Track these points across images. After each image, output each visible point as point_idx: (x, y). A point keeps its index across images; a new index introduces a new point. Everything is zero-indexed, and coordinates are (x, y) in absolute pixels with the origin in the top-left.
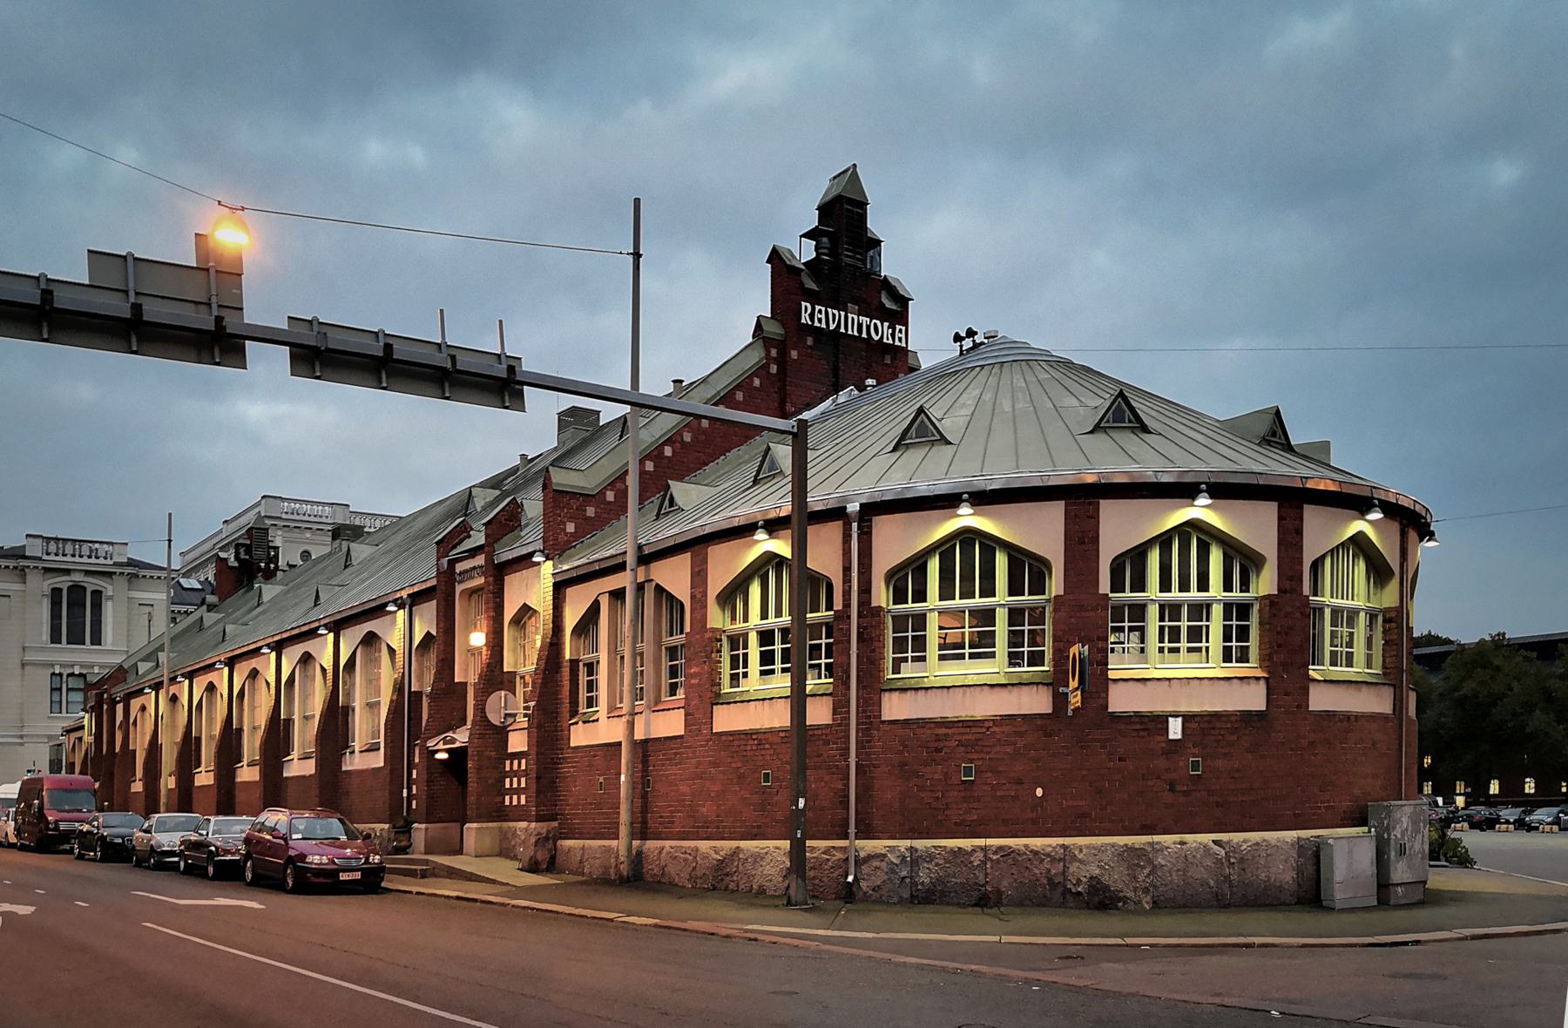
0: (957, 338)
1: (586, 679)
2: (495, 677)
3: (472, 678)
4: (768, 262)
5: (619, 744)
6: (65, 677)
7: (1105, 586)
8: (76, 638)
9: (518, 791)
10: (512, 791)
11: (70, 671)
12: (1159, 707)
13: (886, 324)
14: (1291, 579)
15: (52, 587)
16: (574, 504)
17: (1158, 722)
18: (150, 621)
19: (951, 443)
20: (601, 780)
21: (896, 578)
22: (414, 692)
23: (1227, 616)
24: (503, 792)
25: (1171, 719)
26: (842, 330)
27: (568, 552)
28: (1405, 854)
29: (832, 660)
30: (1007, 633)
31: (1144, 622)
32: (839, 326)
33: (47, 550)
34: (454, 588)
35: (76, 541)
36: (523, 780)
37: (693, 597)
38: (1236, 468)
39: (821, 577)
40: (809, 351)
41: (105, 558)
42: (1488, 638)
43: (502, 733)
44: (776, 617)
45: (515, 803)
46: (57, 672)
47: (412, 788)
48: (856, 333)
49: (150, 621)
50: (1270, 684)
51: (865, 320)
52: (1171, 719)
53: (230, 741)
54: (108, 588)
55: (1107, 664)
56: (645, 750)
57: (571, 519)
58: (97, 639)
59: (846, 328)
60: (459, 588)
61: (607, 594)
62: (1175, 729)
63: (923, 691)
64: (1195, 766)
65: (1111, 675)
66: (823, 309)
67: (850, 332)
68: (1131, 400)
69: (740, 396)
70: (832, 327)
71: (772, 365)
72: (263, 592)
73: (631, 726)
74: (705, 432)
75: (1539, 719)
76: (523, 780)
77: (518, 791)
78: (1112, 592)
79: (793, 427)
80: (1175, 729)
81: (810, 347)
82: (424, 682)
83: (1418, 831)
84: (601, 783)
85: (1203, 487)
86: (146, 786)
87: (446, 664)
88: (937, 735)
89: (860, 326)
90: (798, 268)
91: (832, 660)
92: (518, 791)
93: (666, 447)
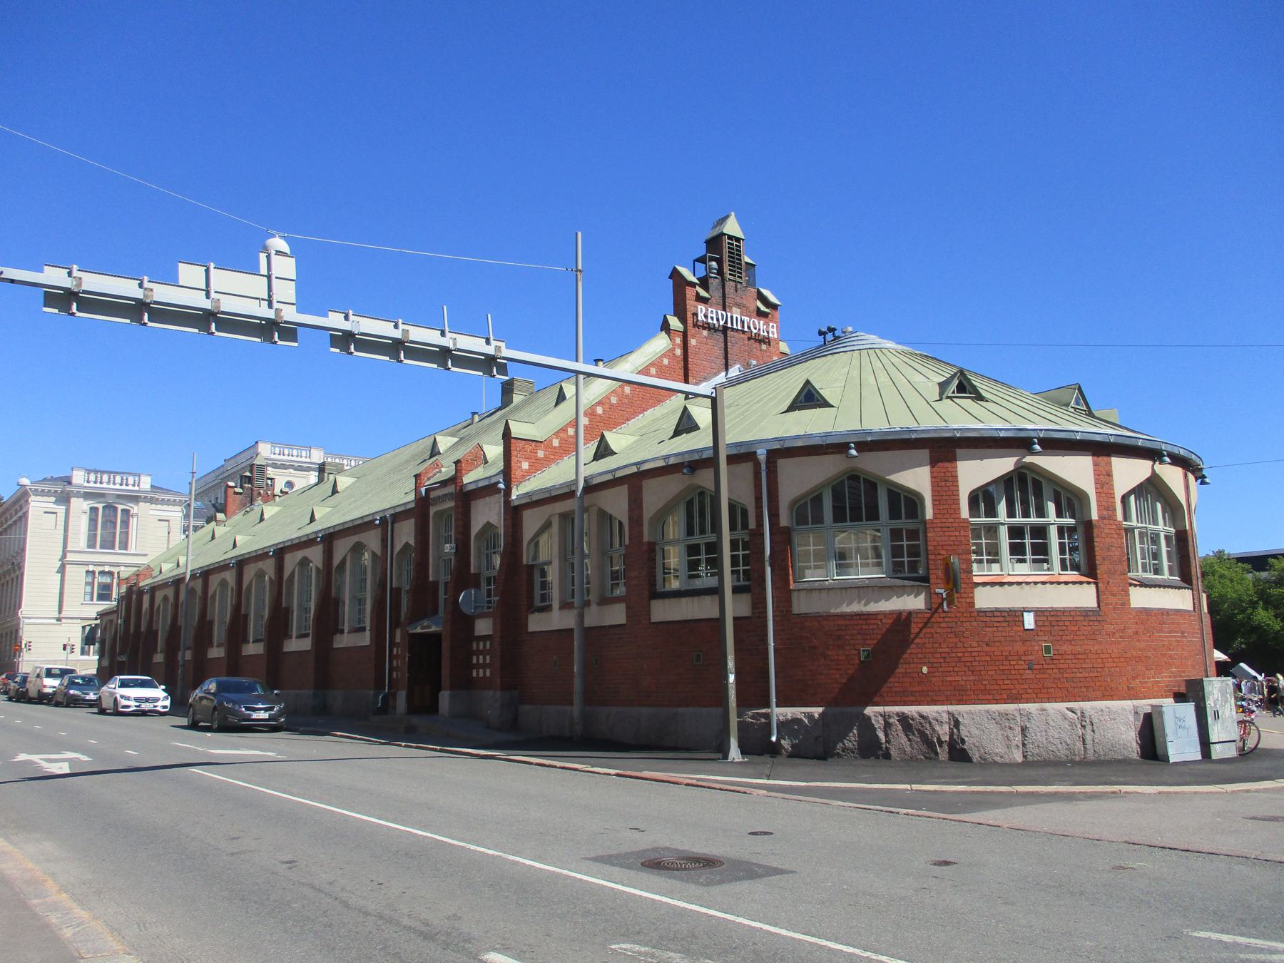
0: (821, 333)
1: (540, 580)
2: (463, 577)
3: (444, 578)
4: (670, 277)
5: (572, 630)
6: (97, 574)
7: (965, 512)
8: (108, 544)
9: (484, 666)
10: (478, 666)
11: (101, 569)
12: (1017, 604)
13: (762, 322)
14: (1107, 509)
15: (90, 506)
16: (528, 448)
17: (1015, 616)
18: (169, 533)
19: (833, 407)
20: (555, 658)
21: (796, 507)
22: (395, 588)
23: (1061, 535)
24: (471, 667)
25: (1025, 614)
26: (729, 325)
27: (523, 483)
28: (1218, 718)
29: (749, 567)
30: (890, 547)
31: (997, 540)
32: (726, 322)
33: (88, 479)
34: (429, 509)
35: (111, 472)
36: (488, 657)
37: (630, 518)
38: (1007, 426)
39: (737, 504)
40: (705, 339)
41: (134, 485)
42: (1211, 554)
43: (468, 622)
44: (700, 534)
45: (481, 675)
46: (91, 570)
47: (393, 663)
48: (739, 328)
49: (169, 533)
50: (1100, 589)
51: (746, 319)
52: (1025, 614)
53: (205, 627)
54: (134, 509)
55: (972, 573)
56: (595, 635)
57: (527, 458)
58: (124, 545)
59: (732, 324)
60: (433, 510)
61: (557, 515)
62: (1029, 621)
63: (826, 591)
64: (1048, 649)
65: (976, 580)
66: (714, 311)
67: (735, 327)
68: (973, 382)
69: (653, 371)
70: (722, 323)
71: (676, 349)
72: (264, 511)
73: (581, 617)
74: (627, 397)
75: (1263, 615)
76: (488, 657)
77: (484, 666)
78: (970, 517)
79: (712, 393)
80: (1029, 621)
81: (705, 337)
82: (401, 578)
83: (1226, 701)
84: (555, 661)
85: (1036, 440)
86: (166, 658)
87: (422, 566)
88: (839, 625)
89: (743, 322)
90: (693, 283)
91: (749, 567)
92: (484, 666)
93: (598, 407)
